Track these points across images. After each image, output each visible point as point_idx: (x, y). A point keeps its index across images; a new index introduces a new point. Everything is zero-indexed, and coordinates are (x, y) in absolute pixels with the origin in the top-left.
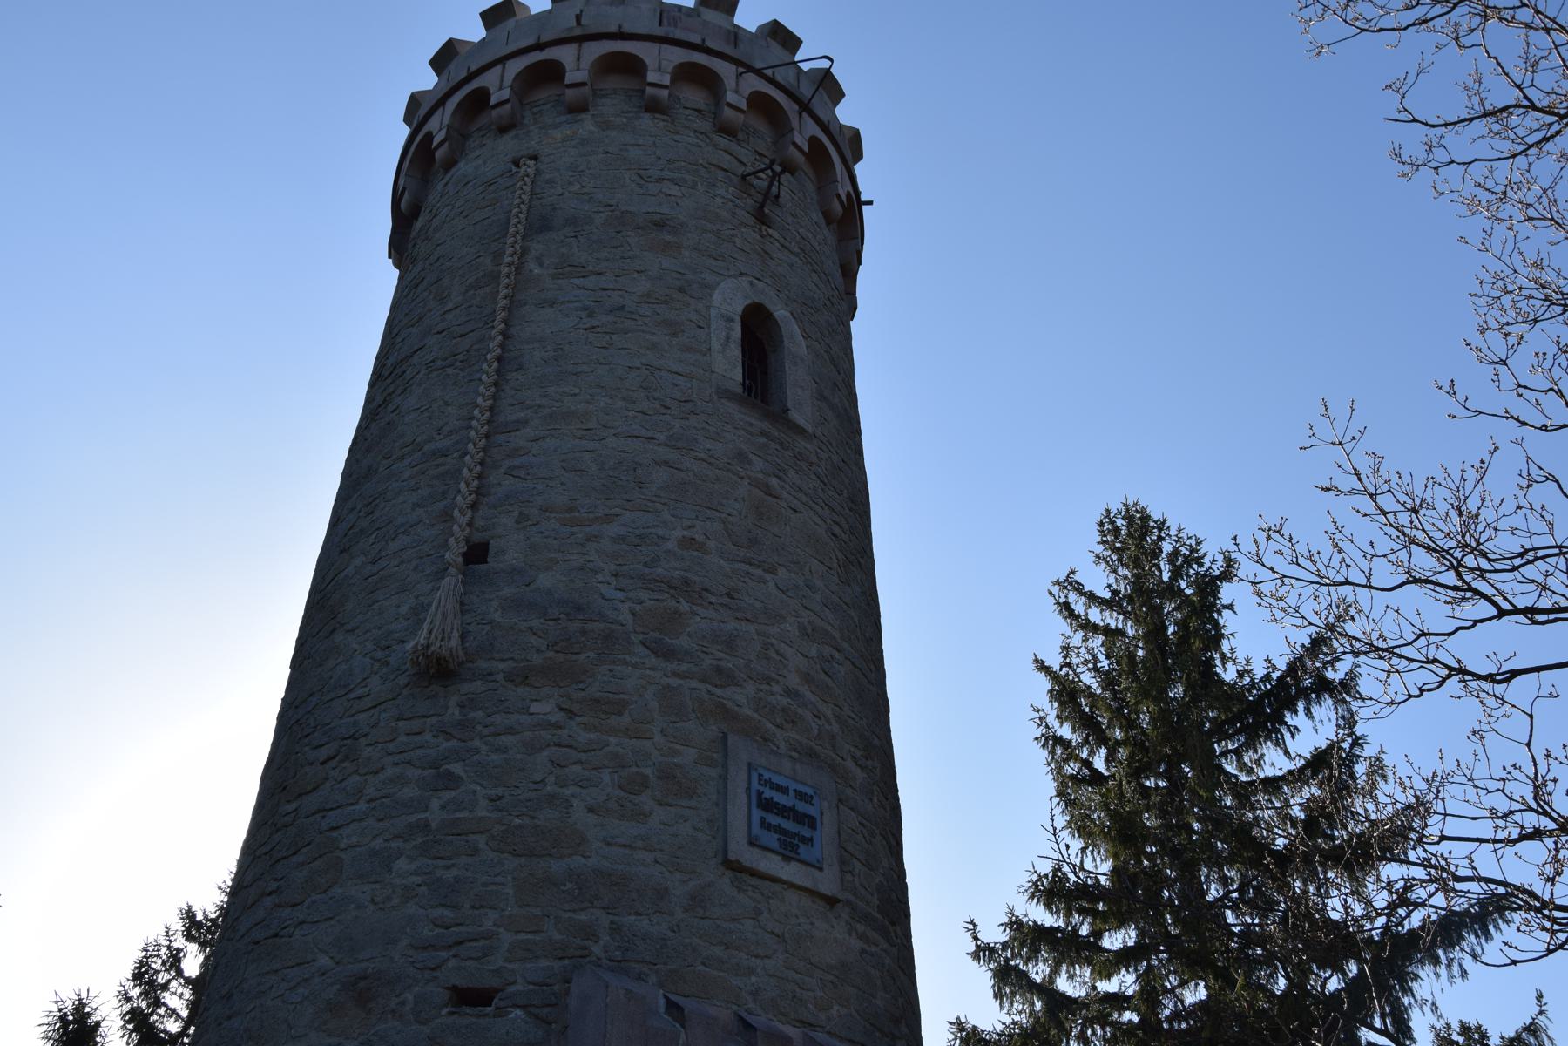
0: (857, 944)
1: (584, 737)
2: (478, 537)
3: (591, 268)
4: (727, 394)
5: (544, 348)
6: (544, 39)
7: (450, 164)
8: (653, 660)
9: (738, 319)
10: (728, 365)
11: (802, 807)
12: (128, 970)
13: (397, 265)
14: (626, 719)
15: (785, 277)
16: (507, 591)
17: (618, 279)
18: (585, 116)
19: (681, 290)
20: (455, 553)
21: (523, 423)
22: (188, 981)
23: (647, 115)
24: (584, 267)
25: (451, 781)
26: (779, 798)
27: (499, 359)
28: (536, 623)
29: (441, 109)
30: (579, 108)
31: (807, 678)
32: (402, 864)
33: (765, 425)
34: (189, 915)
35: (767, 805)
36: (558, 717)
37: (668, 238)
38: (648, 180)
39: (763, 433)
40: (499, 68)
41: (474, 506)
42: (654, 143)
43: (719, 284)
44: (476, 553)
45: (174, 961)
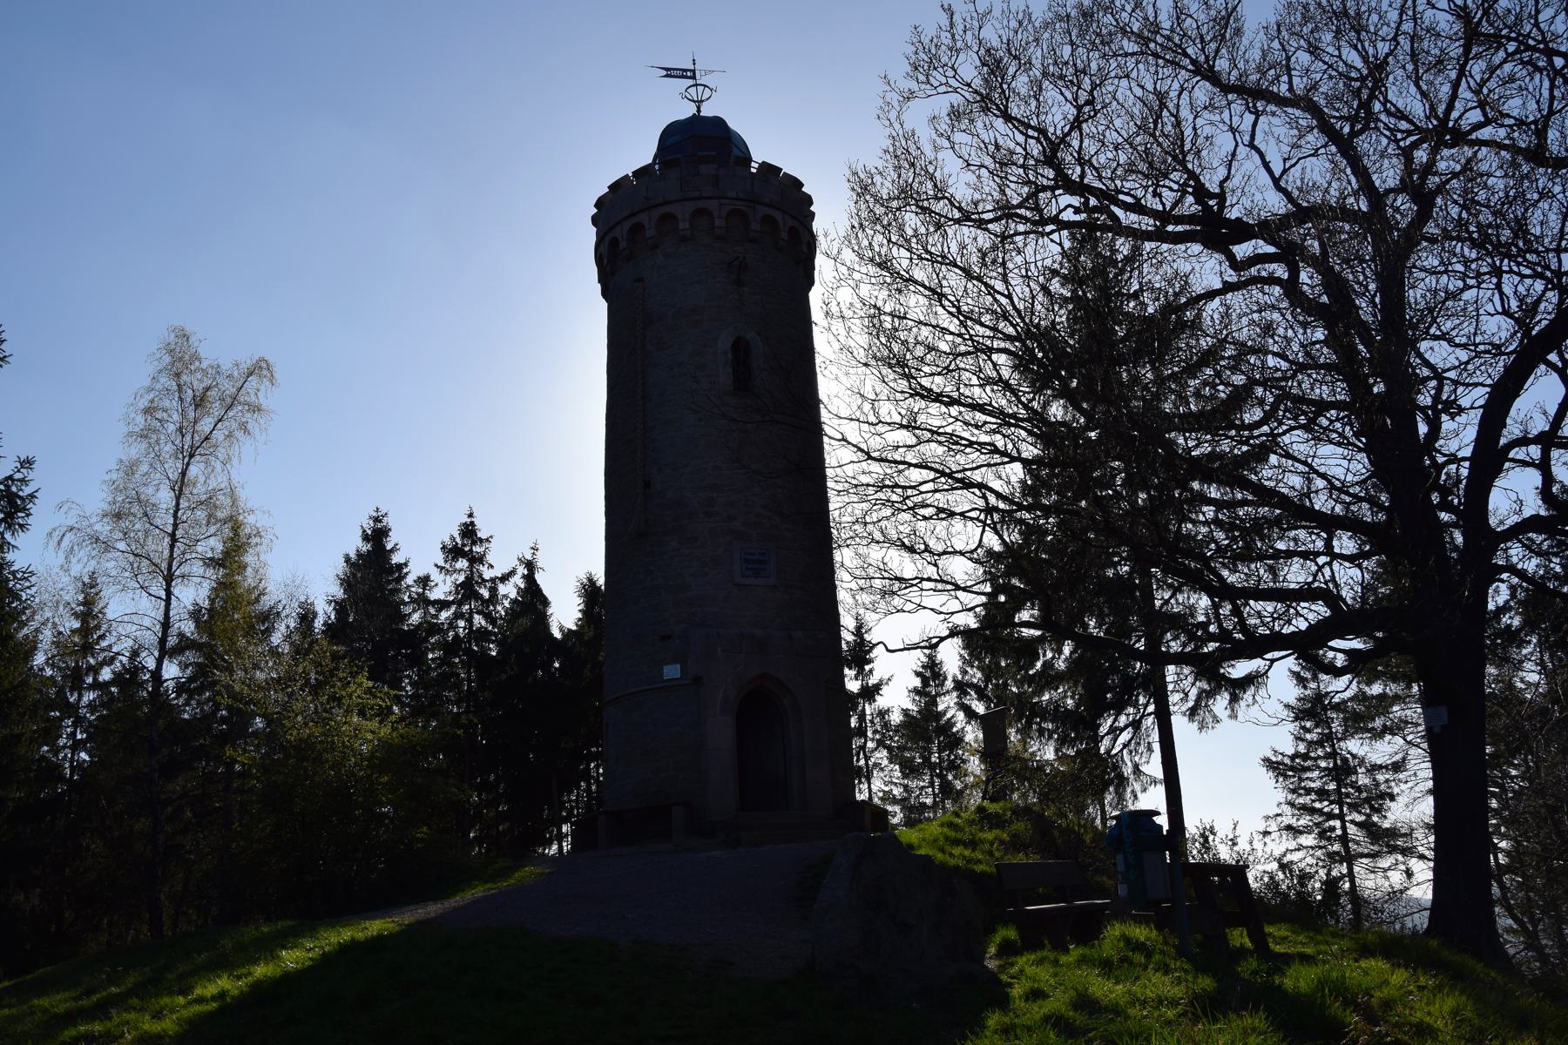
44: (647, 485)
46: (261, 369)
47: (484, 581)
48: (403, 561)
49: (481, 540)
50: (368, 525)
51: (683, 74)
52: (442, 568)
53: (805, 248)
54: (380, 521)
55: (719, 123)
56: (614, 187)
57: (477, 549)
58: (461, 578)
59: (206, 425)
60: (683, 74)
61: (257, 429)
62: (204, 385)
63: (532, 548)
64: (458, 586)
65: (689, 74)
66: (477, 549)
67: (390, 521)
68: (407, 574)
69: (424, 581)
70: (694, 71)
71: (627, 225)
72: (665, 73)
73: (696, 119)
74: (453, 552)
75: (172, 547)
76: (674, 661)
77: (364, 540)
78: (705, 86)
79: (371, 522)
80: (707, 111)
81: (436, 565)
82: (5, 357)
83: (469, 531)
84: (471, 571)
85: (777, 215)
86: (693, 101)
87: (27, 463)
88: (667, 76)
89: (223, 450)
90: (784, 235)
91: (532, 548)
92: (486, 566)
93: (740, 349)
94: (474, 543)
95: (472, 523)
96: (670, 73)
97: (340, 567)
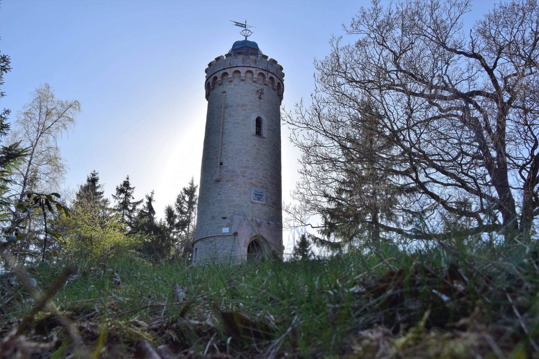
0: (268, 209)
1: (235, 188)
2: (221, 161)
7: (213, 89)
8: (242, 178)
10: (253, 130)
11: (261, 194)
12: (176, 200)
13: (207, 100)
14: (239, 186)
16: (225, 169)
18: (232, 83)
20: (218, 165)
21: (226, 144)
22: (187, 202)
25: (220, 194)
26: (258, 193)
28: (228, 174)
30: (231, 81)
31: (263, 176)
32: (216, 204)
33: (259, 139)
34: (185, 189)
35: (256, 194)
36: (231, 186)
37: (245, 108)
39: (259, 140)
40: (218, 73)
41: (220, 157)
44: (221, 164)
45: (184, 198)
46: (74, 105)
47: (130, 203)
48: (102, 191)
49: (130, 188)
50: (90, 176)
51: (242, 25)
52: (115, 196)
54: (95, 175)
55: (255, 44)
56: (218, 59)
57: (128, 191)
58: (121, 201)
59: (48, 124)
60: (242, 25)
61: (69, 127)
62: (52, 107)
63: (152, 193)
64: (120, 204)
66: (128, 191)
67: (100, 176)
68: (102, 197)
69: (105, 201)
70: (245, 25)
71: (221, 73)
72: (236, 24)
73: (246, 42)
74: (121, 191)
75: (29, 165)
76: (227, 226)
77: (88, 181)
79: (91, 175)
81: (113, 195)
82: (10, 68)
83: (126, 184)
84: (126, 199)
85: (275, 77)
87: (7, 112)
88: (236, 25)
89: (54, 133)
90: (276, 85)
91: (152, 193)
92: (131, 198)
93: (259, 121)
94: (127, 189)
95: (128, 182)
96: (237, 24)
97: (77, 190)
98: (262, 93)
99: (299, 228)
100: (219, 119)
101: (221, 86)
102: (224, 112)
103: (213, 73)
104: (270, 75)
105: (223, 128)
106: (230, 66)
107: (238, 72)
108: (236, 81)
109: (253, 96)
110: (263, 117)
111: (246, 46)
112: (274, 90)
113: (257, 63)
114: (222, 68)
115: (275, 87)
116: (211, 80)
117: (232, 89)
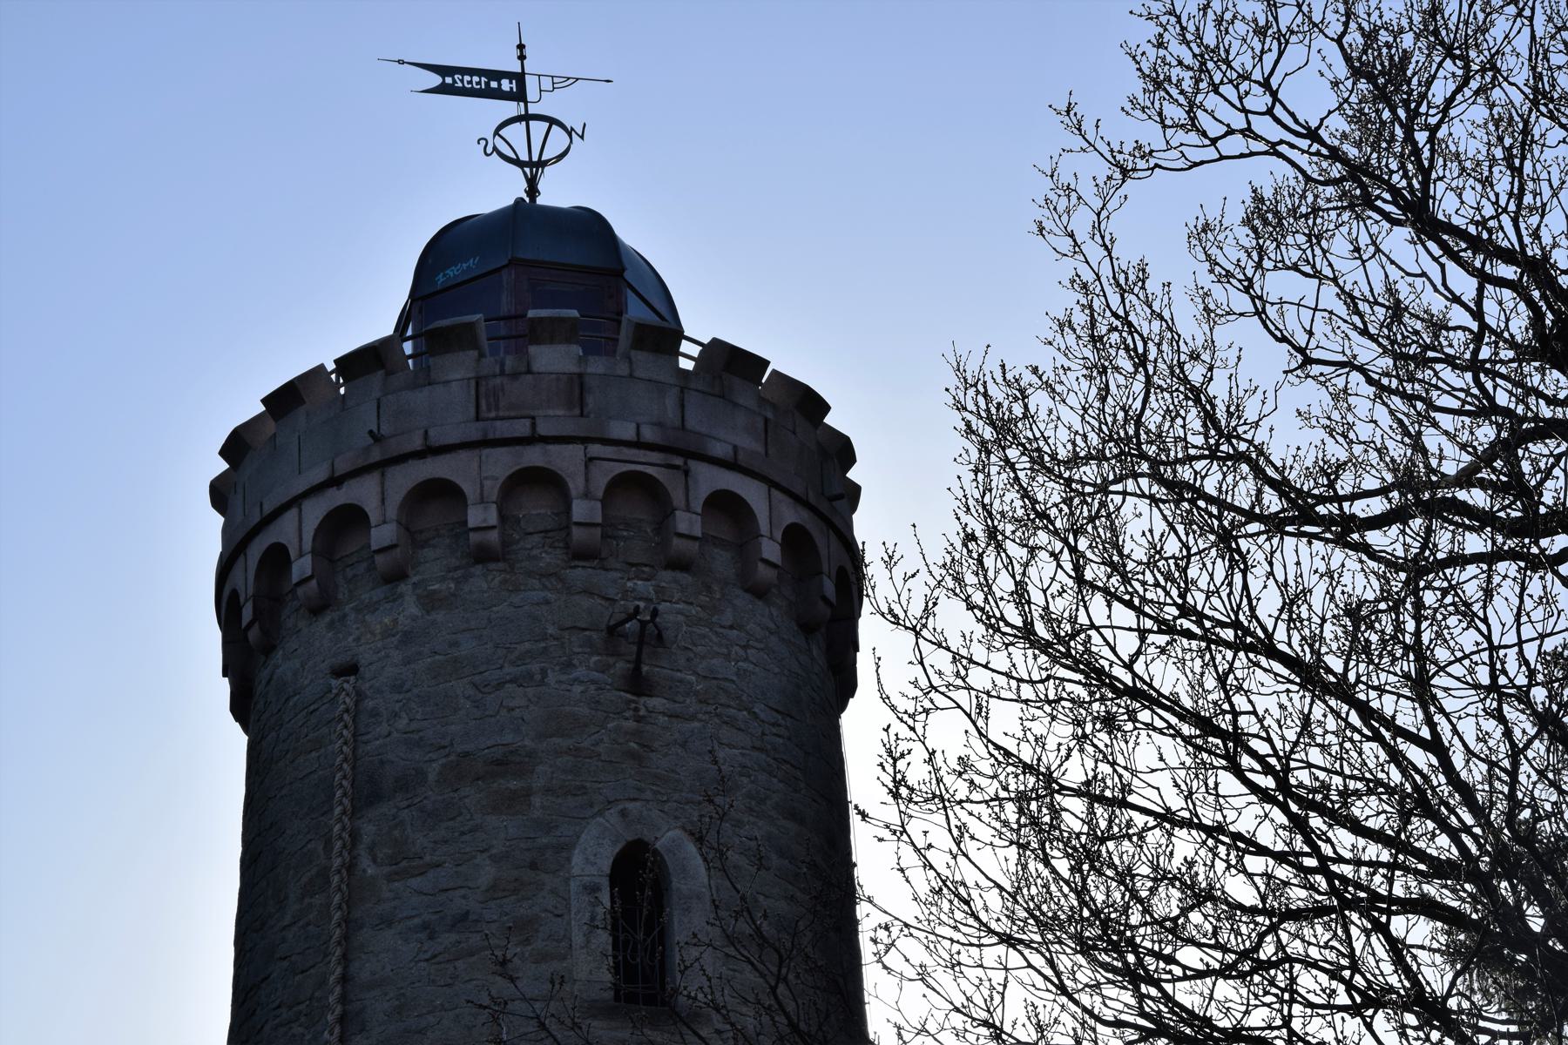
3: (428, 858)
4: (597, 1010)
5: (386, 995)
6: (342, 467)
7: (269, 649)
9: (605, 883)
15: (673, 771)
17: (459, 868)
18: (404, 588)
19: (533, 866)
23: (478, 570)
24: (421, 858)
27: (342, 1020)
29: (241, 558)
30: (396, 576)
37: (514, 784)
38: (486, 690)
40: (292, 514)
42: (490, 621)
43: (578, 837)
53: (829, 588)
65: (506, 85)
70: (520, 78)
71: (315, 512)
72: (436, 80)
78: (552, 121)
80: (556, 192)
85: (752, 493)
86: (517, 162)
88: (442, 89)
90: (771, 550)
98: (651, 637)
99: (1239, 1016)
100: (318, 900)
101: (327, 618)
102: (355, 836)
103: (256, 519)
104: (710, 480)
105: (344, 979)
106: (376, 455)
107: (442, 492)
108: (434, 565)
109: (580, 672)
110: (671, 839)
111: (514, 263)
112: (759, 592)
113: (590, 401)
114: (319, 474)
115: (764, 573)
116: (245, 578)
117: (407, 638)
